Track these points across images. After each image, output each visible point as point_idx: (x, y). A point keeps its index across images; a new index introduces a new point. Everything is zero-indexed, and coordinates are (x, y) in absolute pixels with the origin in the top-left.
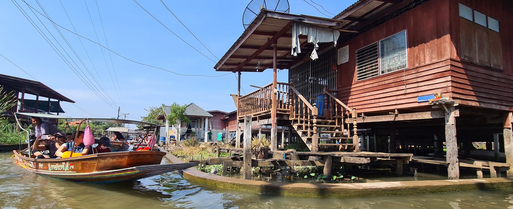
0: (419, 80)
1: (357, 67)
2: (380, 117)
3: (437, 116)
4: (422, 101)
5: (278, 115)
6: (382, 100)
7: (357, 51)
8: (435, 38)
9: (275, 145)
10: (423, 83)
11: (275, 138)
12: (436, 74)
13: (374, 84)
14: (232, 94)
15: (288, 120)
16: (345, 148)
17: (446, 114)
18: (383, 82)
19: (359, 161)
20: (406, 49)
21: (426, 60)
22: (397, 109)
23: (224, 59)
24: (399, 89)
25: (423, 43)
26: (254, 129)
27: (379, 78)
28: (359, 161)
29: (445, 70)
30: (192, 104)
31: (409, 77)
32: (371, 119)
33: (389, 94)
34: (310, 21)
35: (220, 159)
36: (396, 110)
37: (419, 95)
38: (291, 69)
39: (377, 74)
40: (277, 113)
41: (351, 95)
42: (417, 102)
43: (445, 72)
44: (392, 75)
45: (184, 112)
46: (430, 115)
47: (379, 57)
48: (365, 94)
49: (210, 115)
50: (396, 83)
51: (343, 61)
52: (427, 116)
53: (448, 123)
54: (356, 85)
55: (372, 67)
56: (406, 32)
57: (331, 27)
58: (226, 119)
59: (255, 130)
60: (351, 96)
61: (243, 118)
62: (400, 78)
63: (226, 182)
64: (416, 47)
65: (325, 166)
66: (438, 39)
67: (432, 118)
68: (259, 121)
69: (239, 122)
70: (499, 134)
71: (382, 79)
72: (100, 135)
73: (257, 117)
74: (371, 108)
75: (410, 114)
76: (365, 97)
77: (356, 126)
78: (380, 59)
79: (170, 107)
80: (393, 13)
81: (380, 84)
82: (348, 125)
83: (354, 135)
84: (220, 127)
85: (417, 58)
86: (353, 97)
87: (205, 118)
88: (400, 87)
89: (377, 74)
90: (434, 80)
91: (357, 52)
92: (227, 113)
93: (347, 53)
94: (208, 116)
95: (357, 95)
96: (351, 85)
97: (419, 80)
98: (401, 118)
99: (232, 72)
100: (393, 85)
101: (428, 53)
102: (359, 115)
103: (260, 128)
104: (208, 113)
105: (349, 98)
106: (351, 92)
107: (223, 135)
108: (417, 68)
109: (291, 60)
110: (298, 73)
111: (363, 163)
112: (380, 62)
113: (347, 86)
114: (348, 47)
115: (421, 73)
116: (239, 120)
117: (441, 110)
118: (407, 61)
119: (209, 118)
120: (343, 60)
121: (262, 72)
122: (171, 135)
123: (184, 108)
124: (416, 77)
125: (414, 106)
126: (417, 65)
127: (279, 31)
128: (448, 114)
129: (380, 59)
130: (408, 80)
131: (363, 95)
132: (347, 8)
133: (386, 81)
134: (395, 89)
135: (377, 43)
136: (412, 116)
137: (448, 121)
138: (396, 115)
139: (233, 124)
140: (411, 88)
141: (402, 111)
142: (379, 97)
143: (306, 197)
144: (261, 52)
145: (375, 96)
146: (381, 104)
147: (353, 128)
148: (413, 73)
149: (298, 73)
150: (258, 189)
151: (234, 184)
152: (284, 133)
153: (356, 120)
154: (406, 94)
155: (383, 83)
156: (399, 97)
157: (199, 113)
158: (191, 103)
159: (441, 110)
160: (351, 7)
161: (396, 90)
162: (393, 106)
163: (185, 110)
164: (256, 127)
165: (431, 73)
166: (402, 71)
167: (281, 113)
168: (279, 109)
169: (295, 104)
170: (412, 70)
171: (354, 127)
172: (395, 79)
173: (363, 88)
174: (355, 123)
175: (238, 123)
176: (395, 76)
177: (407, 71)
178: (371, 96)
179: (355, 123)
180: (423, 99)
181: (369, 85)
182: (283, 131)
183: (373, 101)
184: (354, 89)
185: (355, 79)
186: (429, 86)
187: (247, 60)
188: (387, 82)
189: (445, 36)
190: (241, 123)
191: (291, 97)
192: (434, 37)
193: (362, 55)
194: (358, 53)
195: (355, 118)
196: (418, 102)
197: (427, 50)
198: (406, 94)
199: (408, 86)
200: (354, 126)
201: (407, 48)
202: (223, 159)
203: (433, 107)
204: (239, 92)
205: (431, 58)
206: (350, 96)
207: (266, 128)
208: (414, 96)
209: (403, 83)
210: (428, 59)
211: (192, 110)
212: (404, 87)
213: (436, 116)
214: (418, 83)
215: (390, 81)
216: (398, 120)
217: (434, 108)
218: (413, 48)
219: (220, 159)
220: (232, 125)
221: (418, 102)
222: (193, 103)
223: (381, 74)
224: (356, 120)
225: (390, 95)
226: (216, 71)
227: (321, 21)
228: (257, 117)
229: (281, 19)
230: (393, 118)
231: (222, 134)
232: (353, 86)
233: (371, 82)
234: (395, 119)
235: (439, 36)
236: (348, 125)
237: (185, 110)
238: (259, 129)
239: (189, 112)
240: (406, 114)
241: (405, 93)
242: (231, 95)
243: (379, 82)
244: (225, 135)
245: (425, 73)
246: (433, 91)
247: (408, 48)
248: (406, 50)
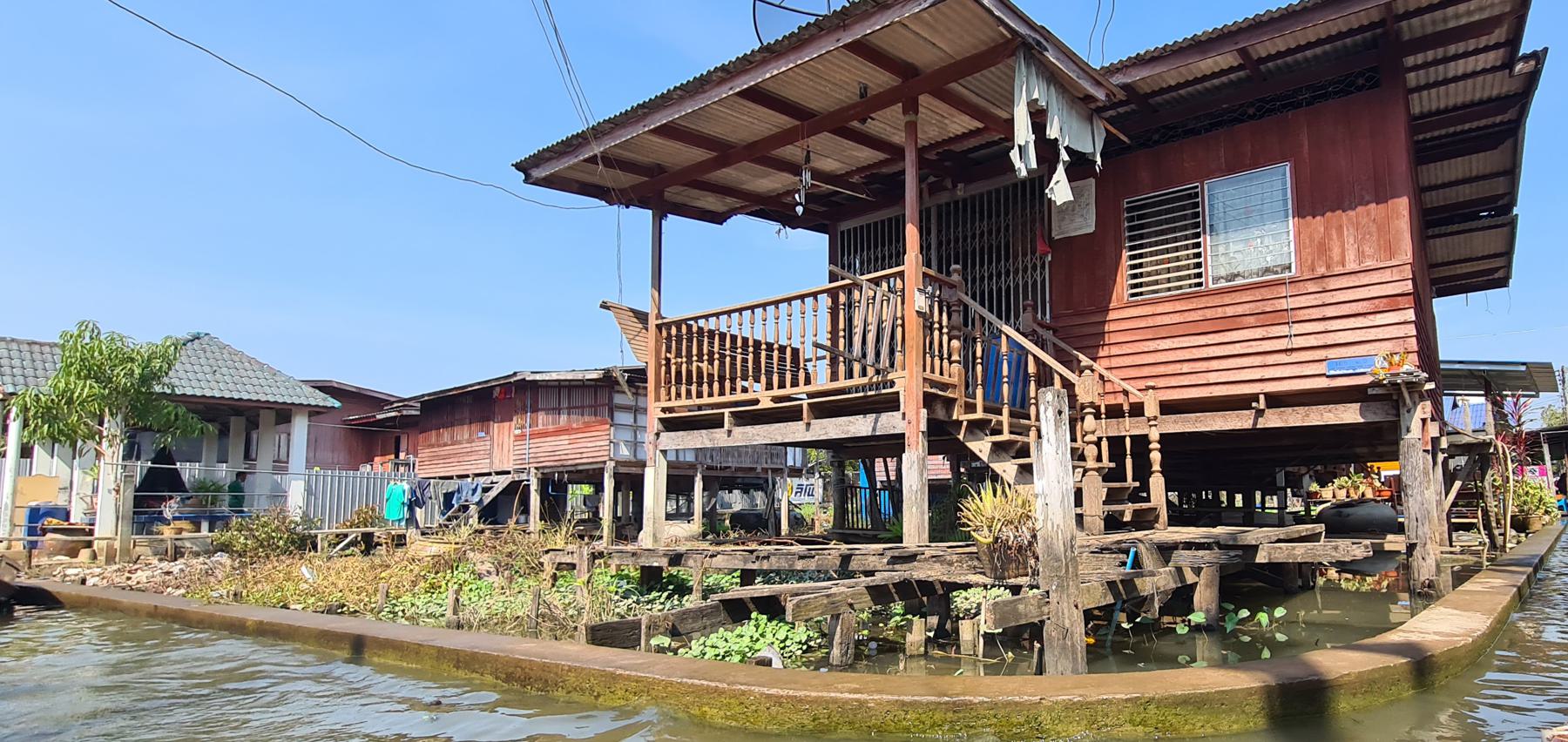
0: (1330, 311)
1: (1126, 254)
2: (1207, 417)
3: (1376, 417)
4: (1338, 372)
5: (929, 401)
6: (1215, 364)
7: (1128, 203)
8: (1372, 202)
9: (924, 520)
10: (1339, 321)
11: (924, 493)
12: (1376, 301)
13: (1187, 313)
14: (612, 300)
15: (947, 419)
16: (1125, 520)
17: (1403, 411)
18: (1220, 309)
19: (1334, 554)
20: (1291, 218)
21: (1347, 258)
22: (1265, 394)
23: (604, 134)
24: (1270, 335)
25: (1338, 209)
26: (577, 465)
27: (1206, 298)
28: (1334, 554)
29: (1399, 291)
30: (197, 337)
31: (1300, 302)
32: (1175, 422)
33: (1237, 349)
34: (1058, 59)
35: (831, 599)
36: (1262, 398)
37: (1330, 357)
38: (842, 233)
39: (1200, 284)
40: (924, 392)
41: (1107, 342)
42: (1324, 375)
43: (1400, 298)
44: (1248, 292)
45: (156, 376)
46: (1358, 412)
47: (1205, 233)
48: (1158, 342)
49: (324, 400)
50: (1261, 316)
51: (1076, 230)
52: (1350, 414)
53: (1409, 436)
54: (1123, 314)
55: (1178, 259)
56: (1288, 168)
57: (1089, 98)
58: (380, 420)
59: (580, 468)
60: (1105, 348)
61: (674, 412)
62: (1271, 302)
63: (1104, 702)
64: (1318, 218)
65: (1202, 582)
66: (1379, 206)
67: (1362, 421)
68: (813, 421)
69: (661, 427)
70: (1290, 469)
71: (1217, 300)
72: (1430, 448)
73: (723, 414)
74: (1178, 390)
75: (1301, 410)
76: (1159, 354)
77: (1159, 446)
78: (1208, 238)
79: (26, 347)
80: (1248, 107)
81: (1209, 314)
82: (1128, 440)
83: (1152, 473)
84: (342, 456)
85: (1323, 249)
86: (1115, 350)
87: (283, 414)
88: (1274, 328)
89: (1200, 284)
90: (1371, 317)
91: (1125, 206)
92: (393, 399)
93: (1087, 205)
94: (309, 405)
95: (1128, 345)
96: (1107, 310)
97: (1330, 311)
98: (1274, 419)
99: (603, 203)
100: (1251, 320)
101: (1352, 241)
102: (1167, 408)
103: (611, 460)
104: (308, 390)
105: (1098, 352)
106: (1106, 335)
107: (413, 492)
108: (1323, 277)
109: (864, 196)
110: (856, 252)
111: (1347, 559)
112: (1209, 248)
113: (1093, 313)
114: (1094, 185)
115: (1334, 293)
116: (660, 419)
117: (1391, 399)
118: (1293, 254)
119: (315, 412)
120: (1075, 225)
121: (721, 224)
122: (33, 504)
123: (164, 357)
124: (1320, 303)
125: (1315, 387)
126: (1321, 270)
127: (929, 71)
128: (1409, 411)
129: (1208, 238)
130: (1298, 311)
131: (1152, 345)
132: (1142, 52)
133: (1227, 308)
134: (1259, 333)
135: (1197, 187)
136: (1307, 415)
137: (1408, 431)
138: (1260, 413)
139: (445, 445)
140: (1303, 334)
141: (1275, 400)
142: (1205, 356)
143: (1391, 703)
144: (791, 143)
145: (1194, 350)
146: (1213, 378)
147: (1150, 451)
148: (1310, 291)
149: (856, 252)
150: (1255, 705)
151: (1149, 701)
152: (704, 478)
153: (1156, 425)
154: (1292, 350)
155: (1220, 312)
156: (1271, 359)
157: (249, 387)
158: (194, 331)
159: (1391, 399)
160: (1155, 54)
161: (1261, 337)
162: (1252, 385)
163: (170, 368)
164: (584, 455)
165: (1351, 299)
166: (1281, 283)
167: (934, 394)
168: (928, 374)
169: (979, 361)
170: (1309, 282)
171: (1151, 446)
172: (1258, 303)
173: (1150, 322)
174: (1154, 435)
175: (658, 435)
176: (1258, 294)
177: (1293, 285)
178: (1178, 352)
179: (1154, 435)
180: (1343, 369)
181: (1171, 315)
182: (699, 470)
183: (1186, 368)
184: (1117, 323)
185: (1120, 291)
186: (1358, 331)
187: (716, 157)
188: (1230, 311)
189: (1396, 200)
190: (672, 434)
191: (955, 333)
192: (1367, 198)
193: (1140, 217)
194: (1129, 210)
195: (1155, 418)
196: (1328, 377)
197: (1348, 230)
198: (1292, 350)
199: (1297, 328)
200: (1150, 443)
201: (1294, 217)
202: (840, 594)
203: (1370, 391)
204: (657, 294)
205: (1361, 255)
206: (1103, 345)
207: (633, 459)
208: (1317, 358)
209: (1282, 317)
210: (1352, 257)
211: (207, 369)
212: (1284, 330)
213: (1374, 416)
214: (1327, 322)
215: (1239, 310)
216: (1267, 426)
217: (1374, 392)
218: (1309, 218)
219: (831, 599)
220: (439, 446)
221: (1328, 377)
222: (203, 331)
223: (1211, 286)
224: (1156, 425)
225: (1241, 352)
226: (526, 181)
227: (1081, 72)
228: (723, 414)
229: (998, 18)
230: (1251, 422)
231: (406, 487)
232: (1112, 315)
233: (1179, 306)
234: (1255, 423)
235: (1381, 199)
236: (1128, 440)
237: (165, 366)
238: (605, 462)
239: (190, 380)
240: (1290, 409)
241: (1289, 347)
242: (605, 306)
243: (1206, 310)
244: (422, 494)
245: (1345, 293)
246: (1367, 346)
247: (1296, 219)
248: (1291, 222)
